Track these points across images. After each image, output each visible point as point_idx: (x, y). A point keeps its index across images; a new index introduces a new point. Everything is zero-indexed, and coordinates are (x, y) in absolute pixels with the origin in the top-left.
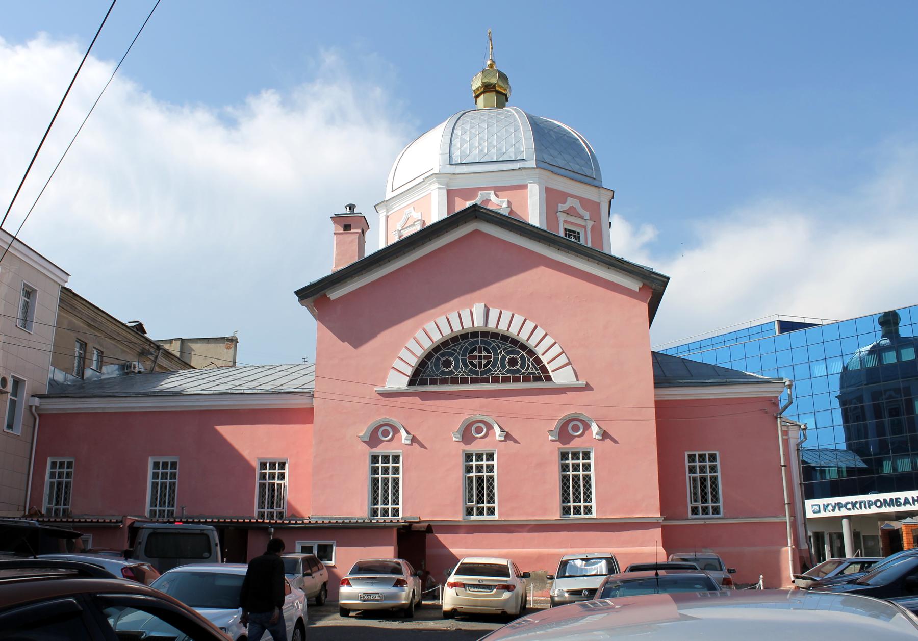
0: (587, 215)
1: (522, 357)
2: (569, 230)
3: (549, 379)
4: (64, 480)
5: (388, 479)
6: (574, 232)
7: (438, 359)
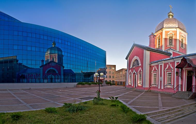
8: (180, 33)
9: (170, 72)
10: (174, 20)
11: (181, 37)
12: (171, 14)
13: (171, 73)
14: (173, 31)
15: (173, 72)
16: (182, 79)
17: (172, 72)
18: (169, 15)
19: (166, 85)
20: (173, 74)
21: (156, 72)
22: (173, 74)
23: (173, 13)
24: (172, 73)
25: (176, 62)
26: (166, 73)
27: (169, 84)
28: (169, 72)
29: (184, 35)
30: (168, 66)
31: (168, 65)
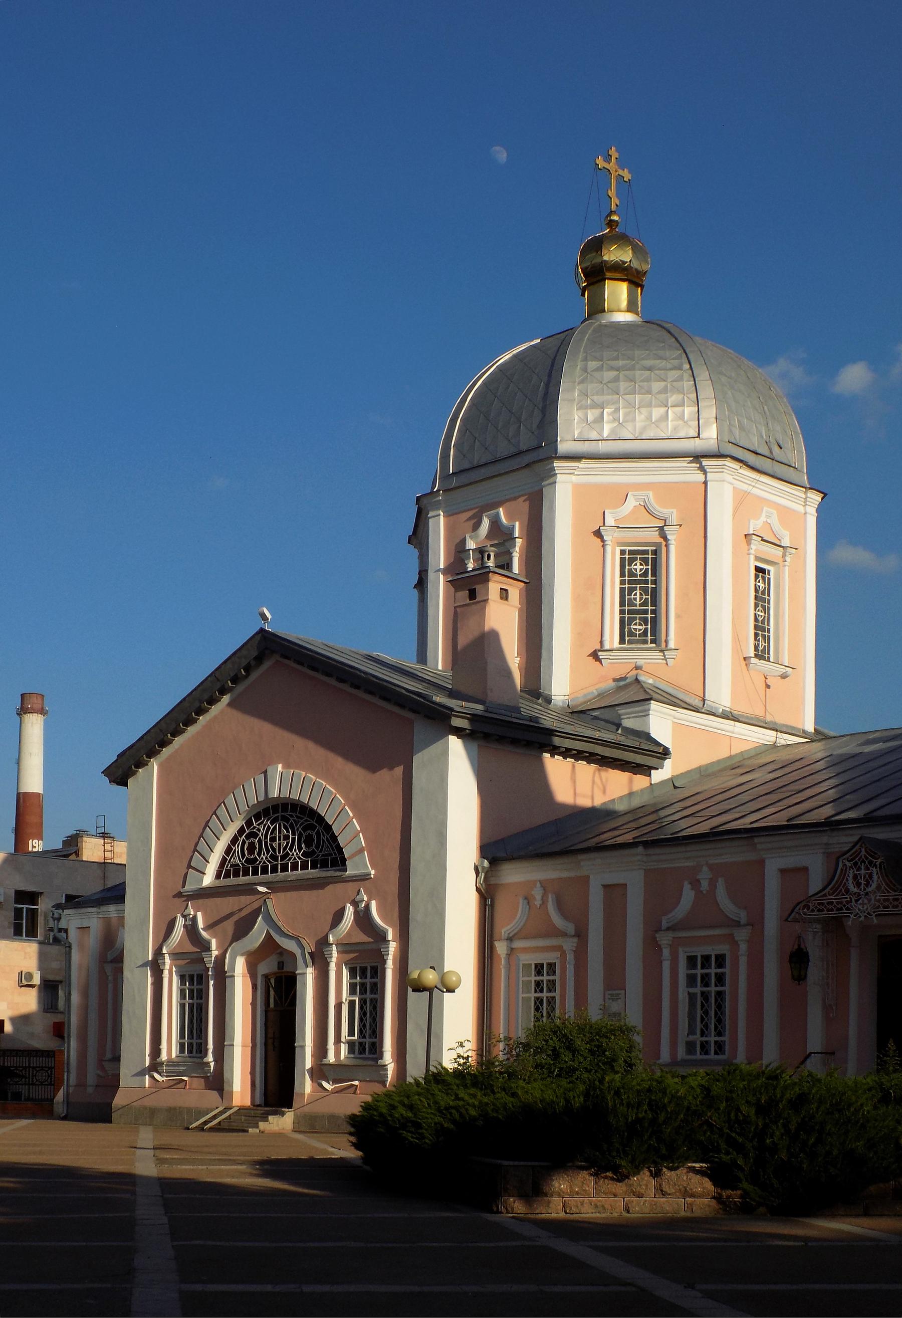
1: (318, 834)
3: (344, 861)
4: (545, 995)
7: (312, 827)
8: (741, 500)
9: (712, 950)
10: (667, 334)
11: (756, 546)
12: (614, 254)
13: (551, 966)
14: (666, 490)
15: (570, 957)
16: (834, 1012)
17: (735, 944)
18: (596, 275)
19: (674, 1063)
20: (743, 961)
21: (559, 948)
22: (743, 961)
23: (636, 249)
24: (736, 959)
25: (773, 866)
26: (666, 952)
27: (704, 1048)
28: (699, 951)
29: (784, 513)
30: (688, 896)
31: (687, 887)
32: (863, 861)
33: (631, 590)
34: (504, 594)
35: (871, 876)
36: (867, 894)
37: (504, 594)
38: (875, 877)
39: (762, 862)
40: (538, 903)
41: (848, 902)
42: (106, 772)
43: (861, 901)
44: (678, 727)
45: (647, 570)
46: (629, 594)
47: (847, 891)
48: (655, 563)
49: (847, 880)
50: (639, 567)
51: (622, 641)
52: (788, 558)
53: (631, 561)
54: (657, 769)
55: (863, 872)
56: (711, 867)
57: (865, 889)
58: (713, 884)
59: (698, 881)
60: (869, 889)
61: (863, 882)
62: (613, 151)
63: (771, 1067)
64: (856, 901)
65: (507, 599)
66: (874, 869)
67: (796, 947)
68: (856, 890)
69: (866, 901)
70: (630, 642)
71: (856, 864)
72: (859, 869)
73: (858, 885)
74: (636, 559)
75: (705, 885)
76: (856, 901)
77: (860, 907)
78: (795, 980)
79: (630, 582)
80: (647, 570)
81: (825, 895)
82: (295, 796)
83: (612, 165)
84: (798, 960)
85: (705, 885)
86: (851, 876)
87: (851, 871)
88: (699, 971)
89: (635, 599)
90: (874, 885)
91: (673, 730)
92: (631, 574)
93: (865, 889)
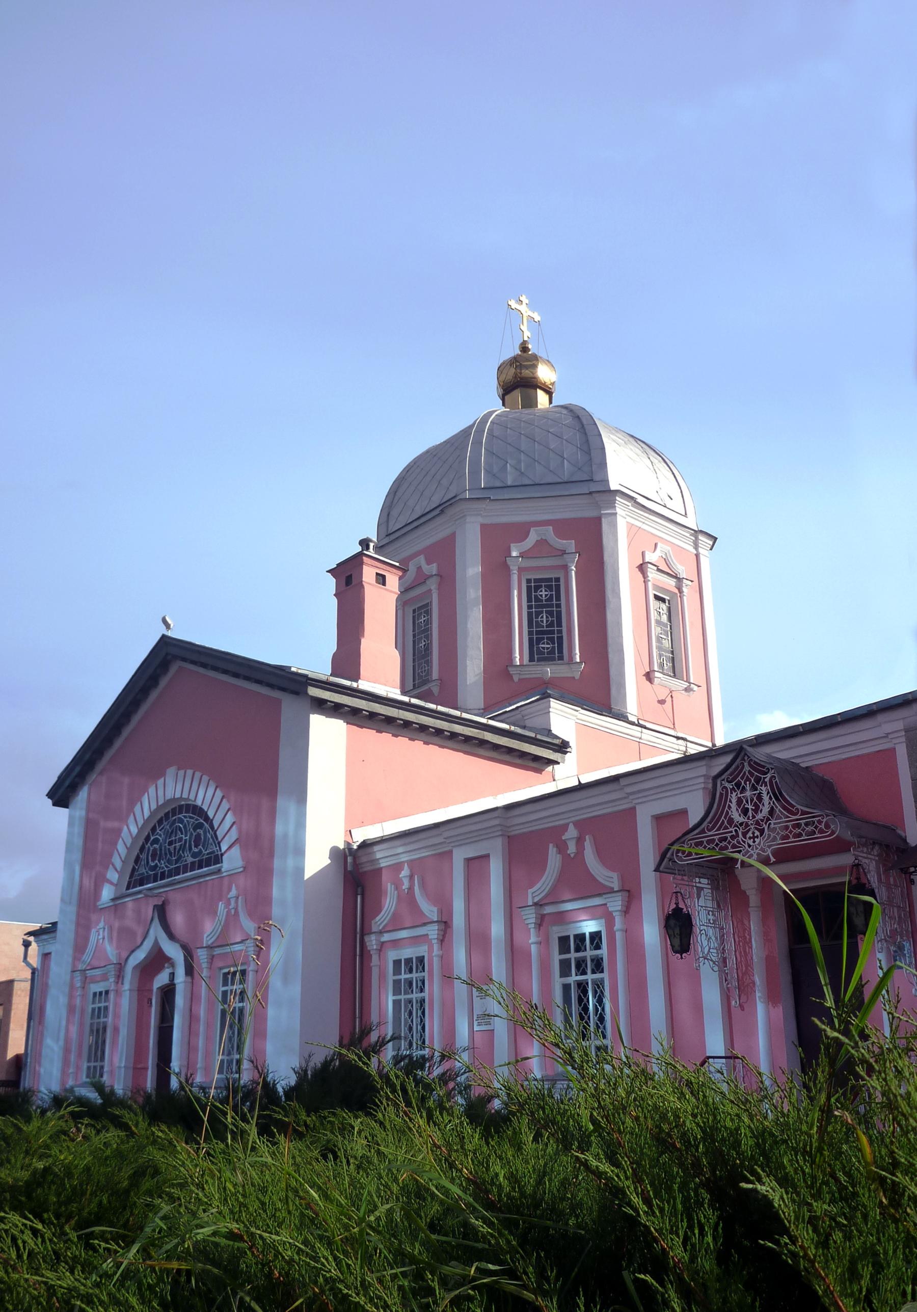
0: (570, 545)
1: (205, 833)
2: (536, 580)
5: (410, 1001)
6: (550, 580)
16: (736, 992)
32: (748, 780)
33: (538, 614)
34: (381, 579)
35: (760, 798)
36: (757, 823)
37: (381, 579)
38: (766, 798)
39: (632, 811)
40: (406, 885)
41: (733, 837)
42: (50, 795)
43: (750, 834)
44: (581, 726)
45: (552, 595)
46: (537, 618)
47: (731, 821)
48: (558, 588)
49: (730, 807)
50: (544, 593)
51: (531, 659)
52: (685, 589)
53: (537, 588)
54: (558, 763)
55: (748, 793)
56: (577, 824)
57: (754, 817)
58: (580, 841)
59: (565, 842)
60: (759, 816)
61: (750, 807)
62: (523, 298)
63: (125, 1112)
64: (744, 834)
65: (384, 584)
66: (763, 788)
67: (673, 906)
68: (741, 819)
69: (757, 833)
70: (539, 660)
71: (738, 785)
72: (744, 789)
73: (745, 812)
74: (541, 586)
75: (572, 849)
76: (744, 834)
77: (751, 842)
78: (676, 952)
79: (552, 632)
80: (552, 595)
81: (703, 832)
82: (199, 802)
83: (523, 308)
84: (679, 928)
85: (572, 849)
86: (734, 800)
87: (734, 794)
88: (573, 955)
89: (542, 621)
90: (766, 810)
91: (577, 730)
92: (537, 599)
93: (754, 817)
